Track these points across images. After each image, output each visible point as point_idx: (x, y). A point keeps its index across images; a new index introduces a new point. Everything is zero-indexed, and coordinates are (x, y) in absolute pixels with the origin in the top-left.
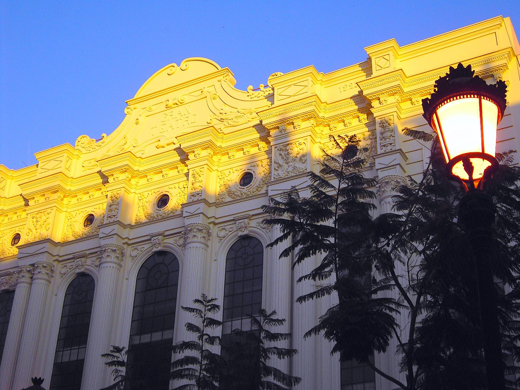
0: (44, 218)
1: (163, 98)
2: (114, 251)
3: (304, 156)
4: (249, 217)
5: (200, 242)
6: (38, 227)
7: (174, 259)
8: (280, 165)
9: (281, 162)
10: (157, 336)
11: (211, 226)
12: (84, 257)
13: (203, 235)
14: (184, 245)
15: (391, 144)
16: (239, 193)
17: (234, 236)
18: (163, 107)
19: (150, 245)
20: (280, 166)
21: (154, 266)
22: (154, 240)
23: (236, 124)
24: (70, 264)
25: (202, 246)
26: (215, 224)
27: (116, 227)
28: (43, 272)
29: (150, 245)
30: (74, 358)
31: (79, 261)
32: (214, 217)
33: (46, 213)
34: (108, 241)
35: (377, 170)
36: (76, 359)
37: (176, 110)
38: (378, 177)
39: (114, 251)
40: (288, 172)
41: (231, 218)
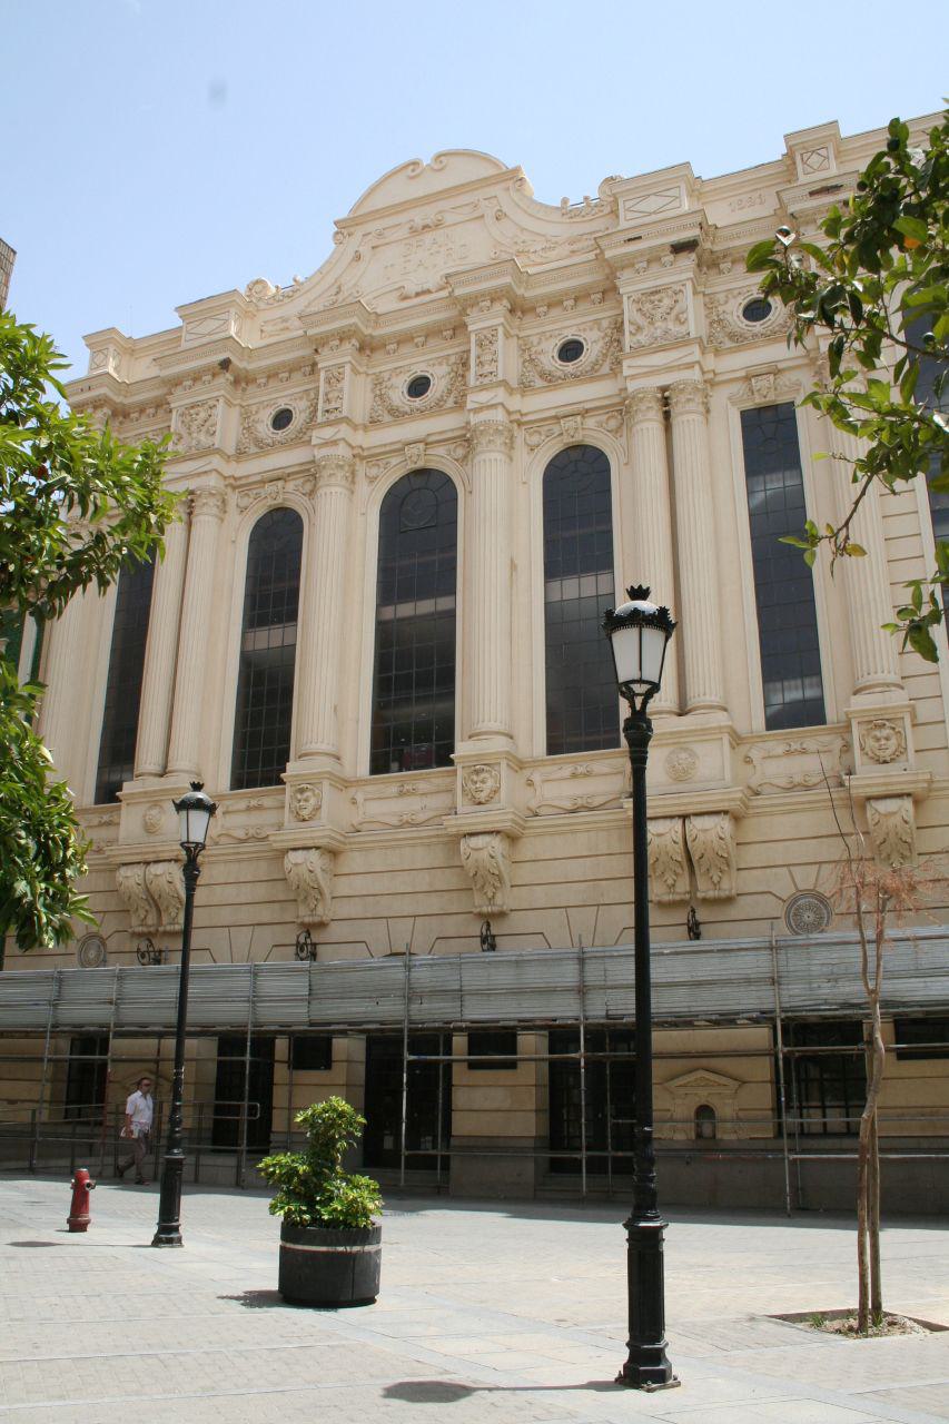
0: (203, 415)
1: (402, 218)
2: (341, 467)
3: (682, 313)
4: (585, 413)
5: (339, 486)
6: (194, 428)
7: (447, 482)
8: (639, 327)
9: (184, 432)
10: (426, 606)
11: (229, 490)
12: (280, 479)
13: (503, 439)
14: (311, 494)
15: (336, 409)
16: (270, 441)
17: (264, 505)
18: (403, 232)
19: (399, 459)
20: (639, 329)
21: (410, 492)
22: (409, 451)
23: (544, 261)
24: (546, 428)
25: (345, 491)
26: (520, 424)
27: (344, 427)
28: (212, 504)
29: (399, 459)
30: (275, 642)
31: (568, 424)
32: (519, 411)
33: (206, 406)
34: (484, 416)
35: (626, 378)
36: (279, 644)
37: (428, 237)
38: (626, 389)
39: (341, 467)
40: (190, 448)
41: (553, 413)
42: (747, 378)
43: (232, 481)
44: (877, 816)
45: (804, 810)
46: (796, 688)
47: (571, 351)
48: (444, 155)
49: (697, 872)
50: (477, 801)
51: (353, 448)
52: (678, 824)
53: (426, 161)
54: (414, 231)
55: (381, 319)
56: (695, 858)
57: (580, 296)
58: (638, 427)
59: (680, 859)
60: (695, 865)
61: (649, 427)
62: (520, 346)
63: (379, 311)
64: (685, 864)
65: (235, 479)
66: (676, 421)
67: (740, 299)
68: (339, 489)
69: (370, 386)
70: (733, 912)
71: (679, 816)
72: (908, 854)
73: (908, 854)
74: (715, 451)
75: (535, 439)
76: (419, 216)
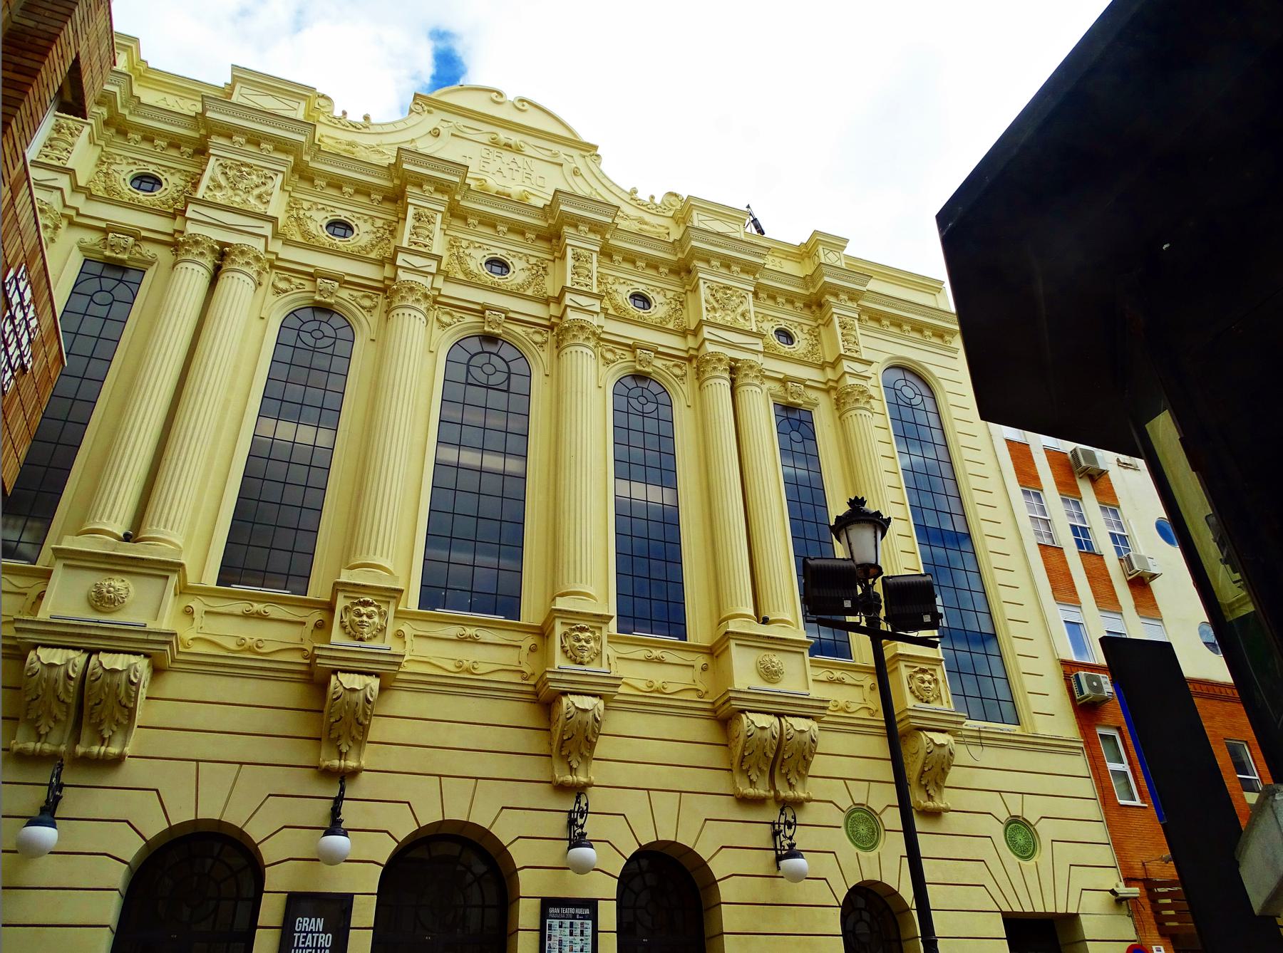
18: (485, 139)
24: (299, 281)
42: (105, 231)
43: (73, 213)
44: (752, 727)
45: (506, 698)
46: (14, 527)
47: (147, 181)
48: (529, 103)
49: (85, 720)
50: (358, 635)
51: (65, 206)
52: (775, 720)
53: (511, 95)
54: (495, 143)
55: (321, 155)
56: (88, 704)
57: (175, 143)
58: (568, 350)
59: (69, 701)
60: (86, 712)
61: (193, 277)
62: (100, 159)
63: (143, 100)
64: (73, 710)
65: (78, 214)
66: (225, 282)
67: (133, 167)
68: (202, 270)
69: (94, 160)
70: (119, 777)
71: (85, 650)
72: (63, 718)
73: (63, 718)
74: (249, 324)
75: (283, 285)
76: (503, 135)
